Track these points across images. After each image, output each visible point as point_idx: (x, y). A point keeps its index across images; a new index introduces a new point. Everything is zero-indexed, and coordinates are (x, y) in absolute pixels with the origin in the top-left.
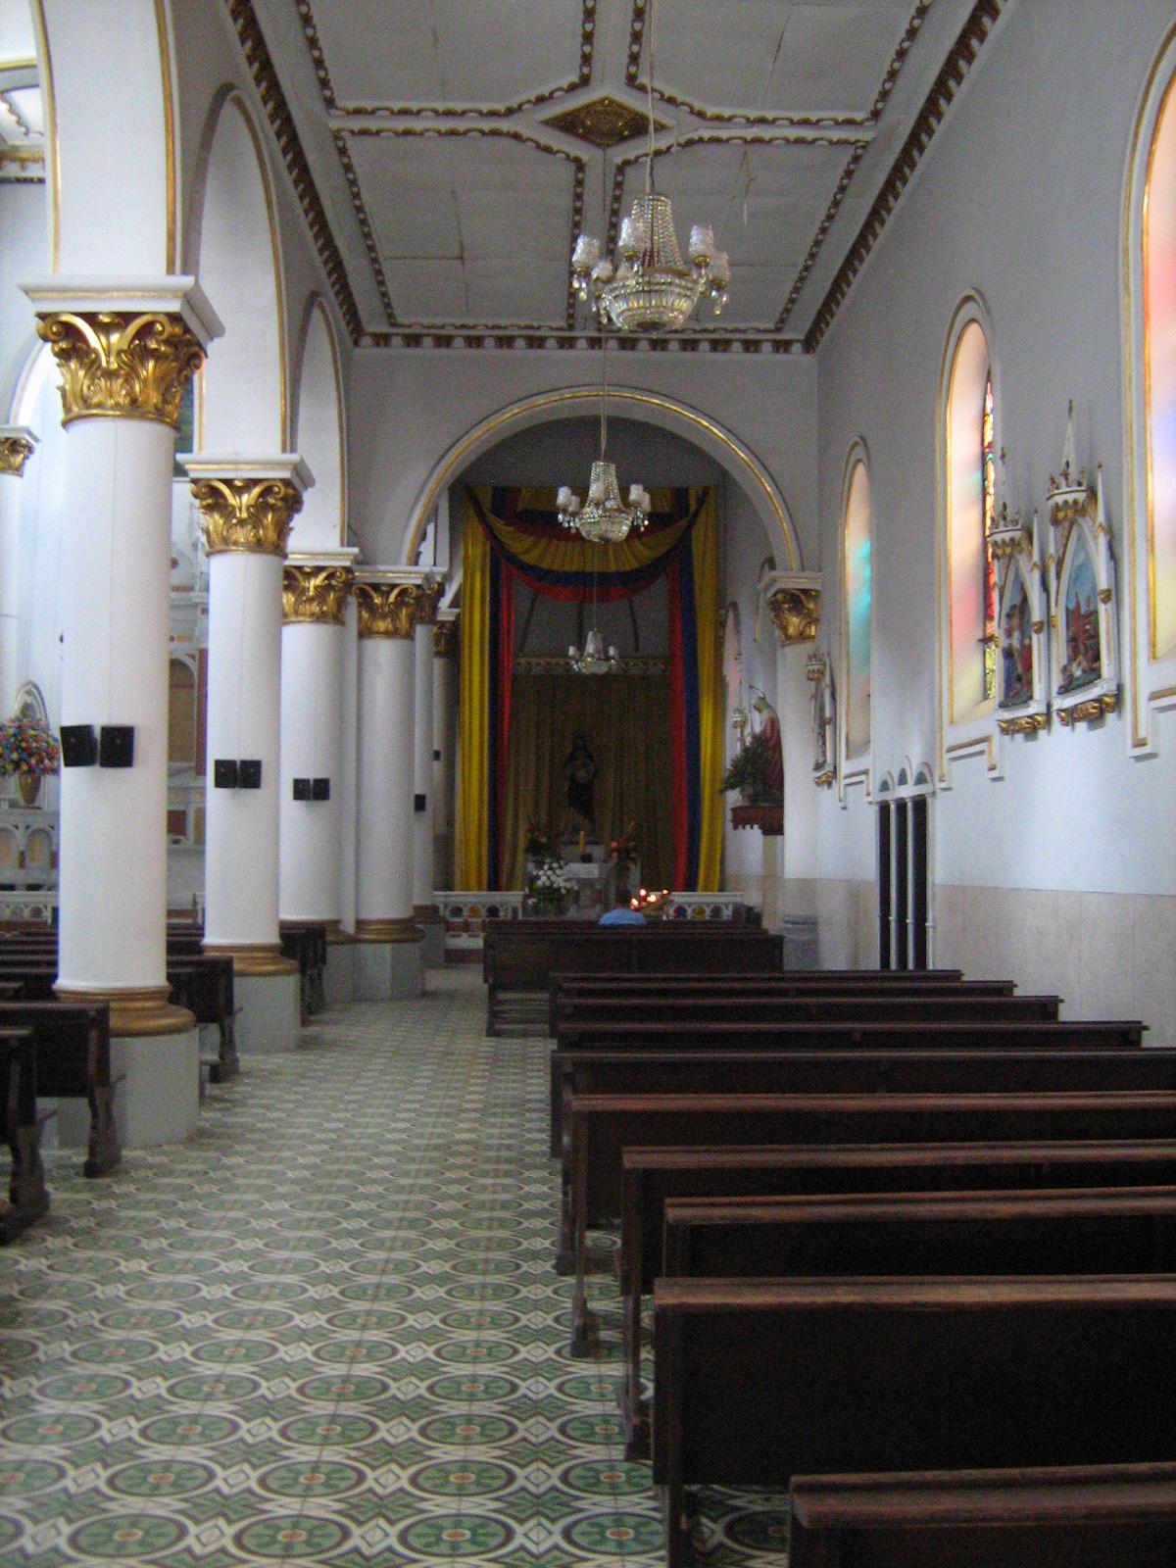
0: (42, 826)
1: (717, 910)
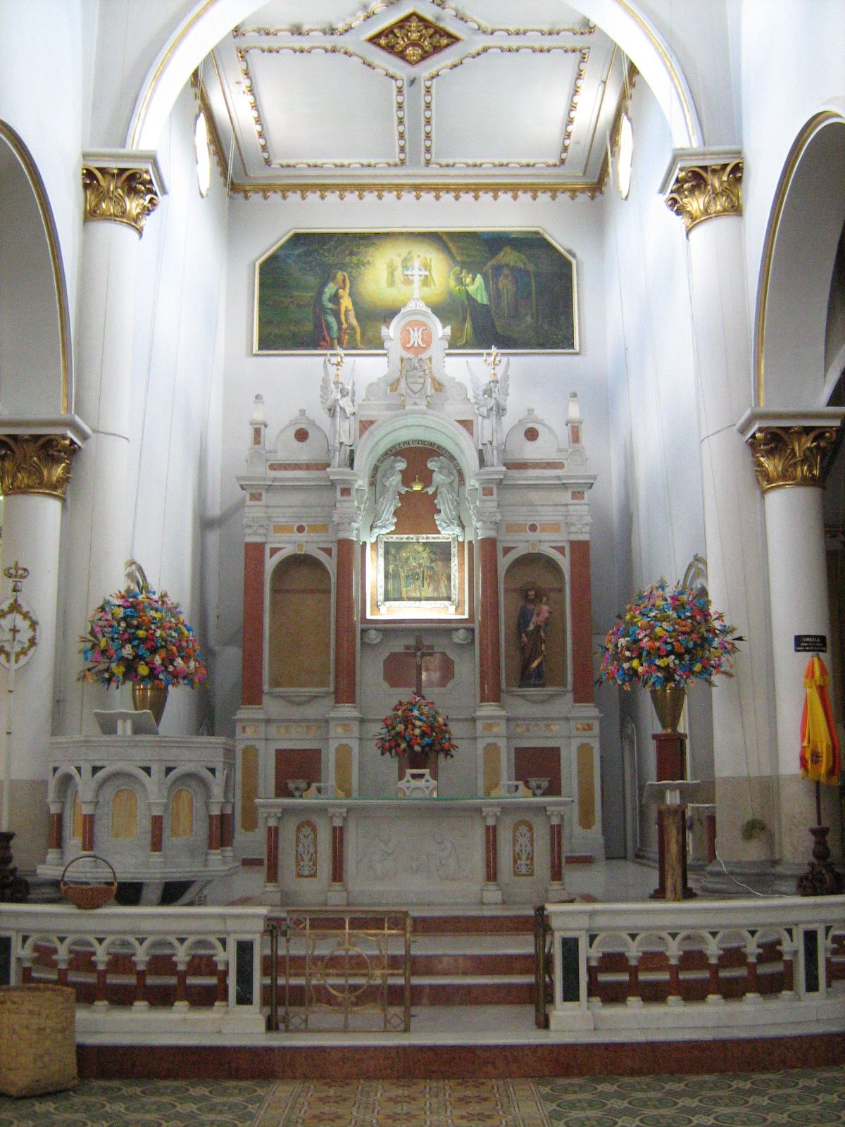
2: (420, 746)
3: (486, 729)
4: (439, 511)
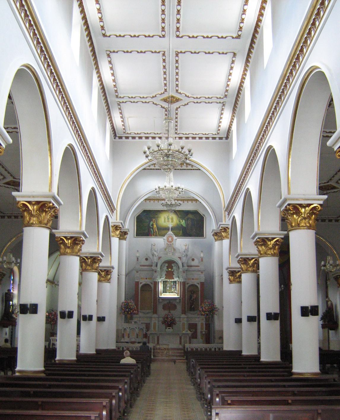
0: (142, 328)
1: (210, 349)
2: (169, 323)
3: (183, 320)
4: (174, 275)
